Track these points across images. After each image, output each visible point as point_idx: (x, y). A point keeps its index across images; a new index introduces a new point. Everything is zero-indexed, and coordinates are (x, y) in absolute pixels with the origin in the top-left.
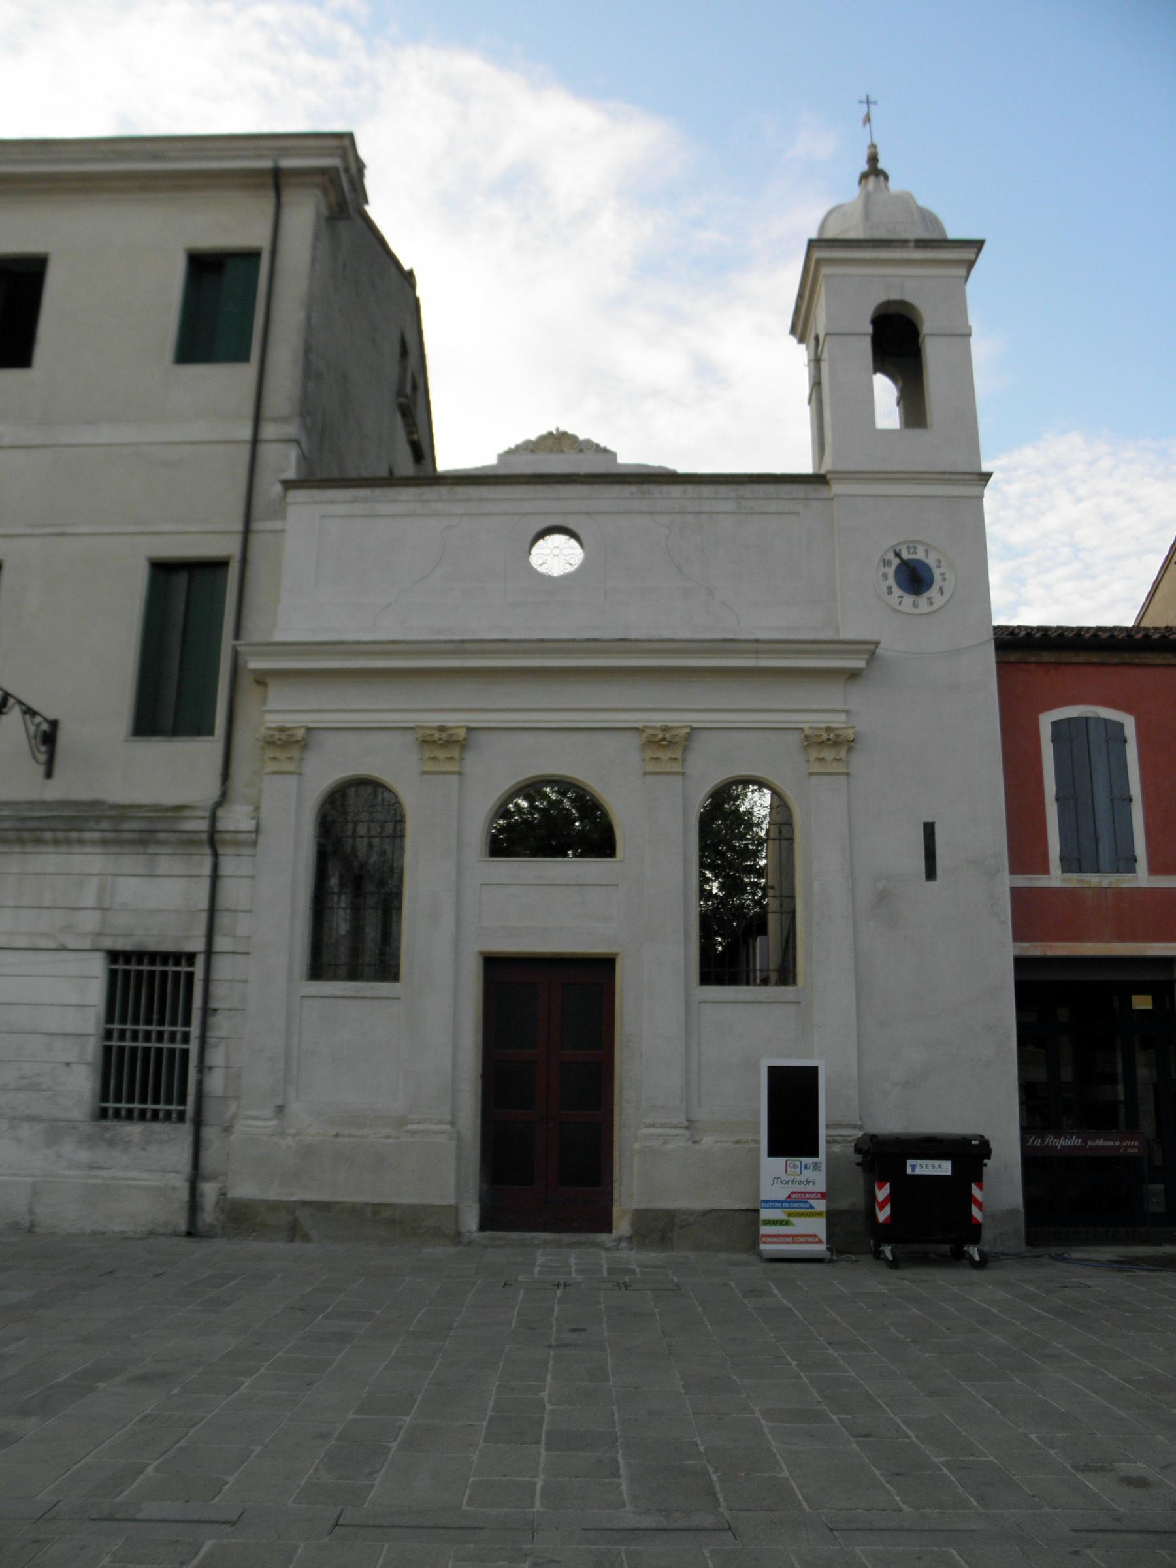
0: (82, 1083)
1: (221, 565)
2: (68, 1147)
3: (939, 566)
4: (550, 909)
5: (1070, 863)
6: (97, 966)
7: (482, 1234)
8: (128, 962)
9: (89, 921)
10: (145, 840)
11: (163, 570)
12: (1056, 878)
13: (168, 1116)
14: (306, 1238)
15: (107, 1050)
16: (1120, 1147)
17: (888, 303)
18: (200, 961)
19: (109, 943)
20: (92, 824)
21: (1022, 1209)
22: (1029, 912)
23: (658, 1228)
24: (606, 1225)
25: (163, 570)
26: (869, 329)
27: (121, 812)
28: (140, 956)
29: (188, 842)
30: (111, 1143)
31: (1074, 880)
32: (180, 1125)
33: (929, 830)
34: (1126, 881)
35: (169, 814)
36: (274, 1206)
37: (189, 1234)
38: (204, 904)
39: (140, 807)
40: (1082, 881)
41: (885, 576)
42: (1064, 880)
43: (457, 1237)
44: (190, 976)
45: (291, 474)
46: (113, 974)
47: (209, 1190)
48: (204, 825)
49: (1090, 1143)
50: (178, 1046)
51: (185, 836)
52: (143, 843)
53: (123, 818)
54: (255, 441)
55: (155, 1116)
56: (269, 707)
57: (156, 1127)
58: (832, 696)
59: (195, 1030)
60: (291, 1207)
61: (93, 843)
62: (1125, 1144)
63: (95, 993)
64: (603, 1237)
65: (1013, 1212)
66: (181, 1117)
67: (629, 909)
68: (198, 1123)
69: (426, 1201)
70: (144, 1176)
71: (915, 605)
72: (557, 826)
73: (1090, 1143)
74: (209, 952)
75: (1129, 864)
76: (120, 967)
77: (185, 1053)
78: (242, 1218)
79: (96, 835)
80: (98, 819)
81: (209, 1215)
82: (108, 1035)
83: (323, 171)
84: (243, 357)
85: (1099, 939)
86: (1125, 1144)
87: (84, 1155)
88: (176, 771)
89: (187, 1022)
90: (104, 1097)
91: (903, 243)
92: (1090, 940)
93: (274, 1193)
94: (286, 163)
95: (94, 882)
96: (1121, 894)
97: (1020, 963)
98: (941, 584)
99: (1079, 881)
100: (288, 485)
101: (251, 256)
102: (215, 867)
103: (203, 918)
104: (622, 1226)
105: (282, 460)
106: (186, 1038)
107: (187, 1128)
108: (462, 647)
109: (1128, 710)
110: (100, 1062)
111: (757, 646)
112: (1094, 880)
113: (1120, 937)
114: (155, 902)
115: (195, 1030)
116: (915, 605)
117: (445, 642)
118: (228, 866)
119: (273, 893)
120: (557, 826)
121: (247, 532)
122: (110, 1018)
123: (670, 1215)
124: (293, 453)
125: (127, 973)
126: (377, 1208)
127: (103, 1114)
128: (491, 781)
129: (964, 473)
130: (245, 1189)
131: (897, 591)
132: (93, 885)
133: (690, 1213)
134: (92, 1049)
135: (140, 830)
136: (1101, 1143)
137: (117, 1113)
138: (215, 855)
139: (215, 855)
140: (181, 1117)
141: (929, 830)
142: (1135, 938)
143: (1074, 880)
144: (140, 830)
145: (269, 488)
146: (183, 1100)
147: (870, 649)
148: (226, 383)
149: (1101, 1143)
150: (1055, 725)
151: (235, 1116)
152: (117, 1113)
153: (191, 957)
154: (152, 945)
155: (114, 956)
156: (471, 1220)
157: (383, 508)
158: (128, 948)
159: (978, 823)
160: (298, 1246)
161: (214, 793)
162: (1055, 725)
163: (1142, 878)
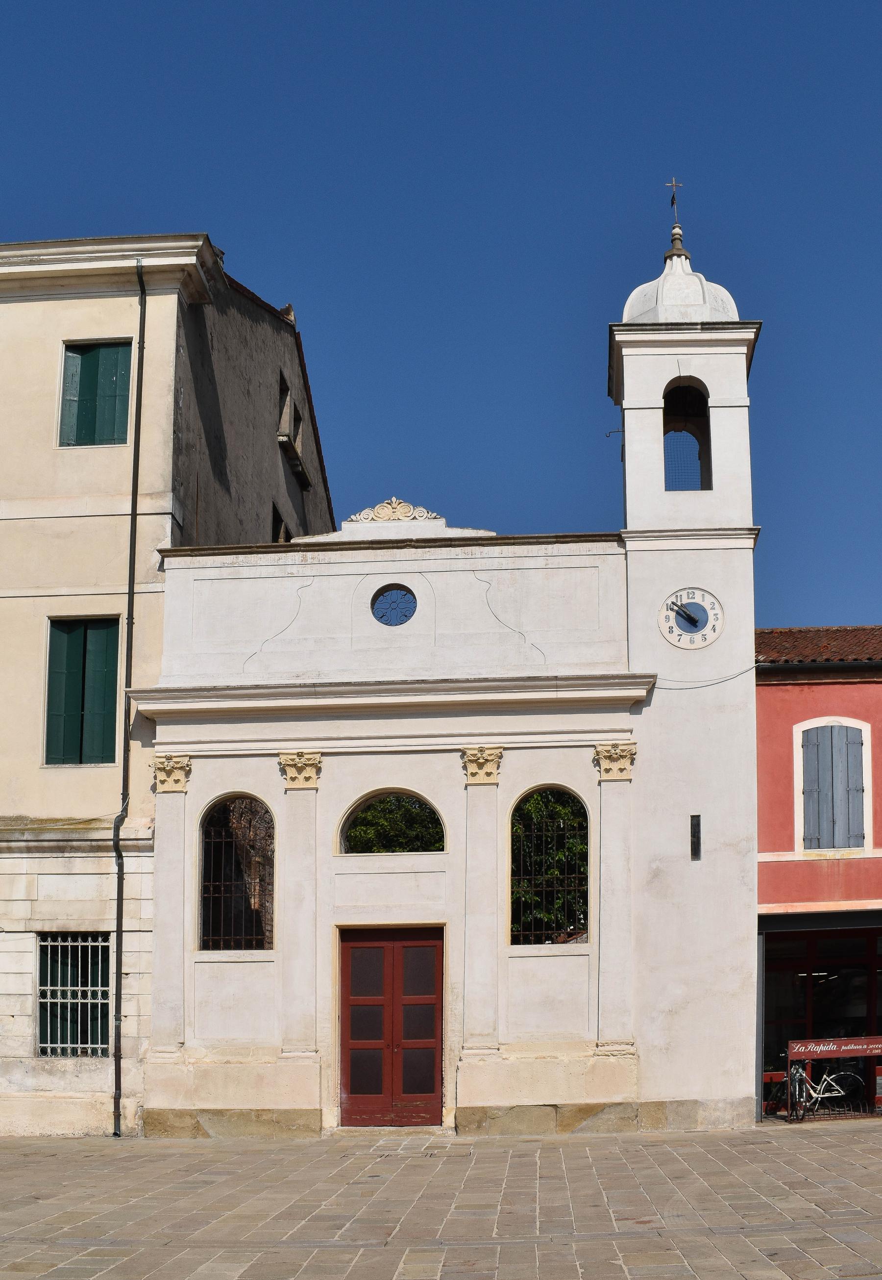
0: (26, 1029)
1: (126, 343)
2: (17, 1075)
3: (713, 608)
4: (392, 889)
5: (811, 842)
6: (32, 944)
7: (340, 1128)
8: (55, 940)
9: (21, 910)
10: (61, 848)
11: (63, 627)
12: (799, 853)
13: (94, 1052)
14: (207, 1135)
15: (43, 1006)
16: (867, 1049)
17: (679, 378)
18: (113, 937)
19: (39, 927)
20: (17, 836)
21: (754, 1097)
22: (773, 879)
23: (474, 1119)
24: (437, 1120)
25: (63, 627)
26: (662, 404)
27: (41, 825)
28: (54, 935)
29: (97, 848)
30: (50, 1072)
31: (814, 854)
32: (105, 1059)
33: (696, 821)
34: (854, 853)
35: (81, 826)
36: (180, 1114)
37: (115, 1134)
38: (115, 896)
39: (57, 821)
40: (821, 855)
41: (667, 618)
42: (805, 855)
43: (344, 1137)
44: (106, 949)
45: (167, 544)
46: (43, 949)
47: (128, 1105)
48: (110, 834)
49: (843, 1048)
50: (100, 1001)
51: (94, 843)
52: (61, 850)
53: (42, 830)
54: (134, 515)
55: (84, 1052)
56: (158, 740)
57: (86, 1060)
58: (621, 719)
59: (112, 989)
60: (191, 1114)
61: (20, 850)
62: (871, 1047)
63: (31, 963)
64: (435, 1128)
65: (748, 1099)
66: (105, 1052)
67: (463, 889)
68: (118, 1057)
69: (297, 1107)
70: (78, 1095)
71: (692, 641)
72: (394, 824)
73: (843, 1048)
74: (120, 932)
75: (858, 839)
76: (49, 943)
77: (105, 1007)
78: (153, 1121)
79: (23, 844)
80: (22, 832)
81: (129, 1122)
82: (43, 994)
83: (182, 268)
84: (109, 758)
85: (831, 898)
86: (871, 1047)
87: (30, 1082)
88: (84, 792)
89: (106, 983)
90: (43, 1040)
91: (690, 326)
92: (823, 900)
93: (180, 1104)
94: (147, 262)
95: (23, 881)
96: (850, 864)
97: (764, 921)
98: (714, 623)
99: (818, 855)
100: (164, 553)
101: (110, 623)
102: (121, 866)
103: (115, 903)
104: (449, 1119)
105: (158, 531)
106: (105, 995)
107: (111, 1061)
108: (313, 690)
109: (865, 719)
110: (38, 1014)
111: (555, 682)
112: (829, 854)
113: (848, 897)
114: (75, 895)
115: (112, 989)
116: (692, 641)
117: (300, 686)
118: (130, 863)
119: (170, 882)
120: (394, 824)
121: (131, 594)
122: (43, 982)
123: (484, 1110)
124: (167, 523)
125: (55, 948)
126: (259, 1113)
127: (44, 1052)
128: (347, 785)
129: (735, 529)
130: (157, 1102)
131: (677, 631)
132: (23, 881)
133: (499, 1108)
134: (31, 1005)
135: (60, 840)
136: (852, 1047)
137: (64, 1050)
138: (120, 857)
139: (120, 857)
140: (105, 1052)
141: (696, 821)
142: (859, 897)
143: (814, 854)
144: (60, 840)
145: (148, 558)
146: (105, 1040)
147: (650, 682)
148: (108, 461)
149: (852, 1047)
150: (806, 733)
151: (146, 1052)
152: (54, 1051)
153: (106, 936)
154: (73, 928)
155: (43, 935)
156: (331, 1118)
157: (245, 572)
158: (54, 930)
159: (734, 815)
160: (200, 1140)
161: (118, 809)
162: (806, 733)
163: (868, 851)
